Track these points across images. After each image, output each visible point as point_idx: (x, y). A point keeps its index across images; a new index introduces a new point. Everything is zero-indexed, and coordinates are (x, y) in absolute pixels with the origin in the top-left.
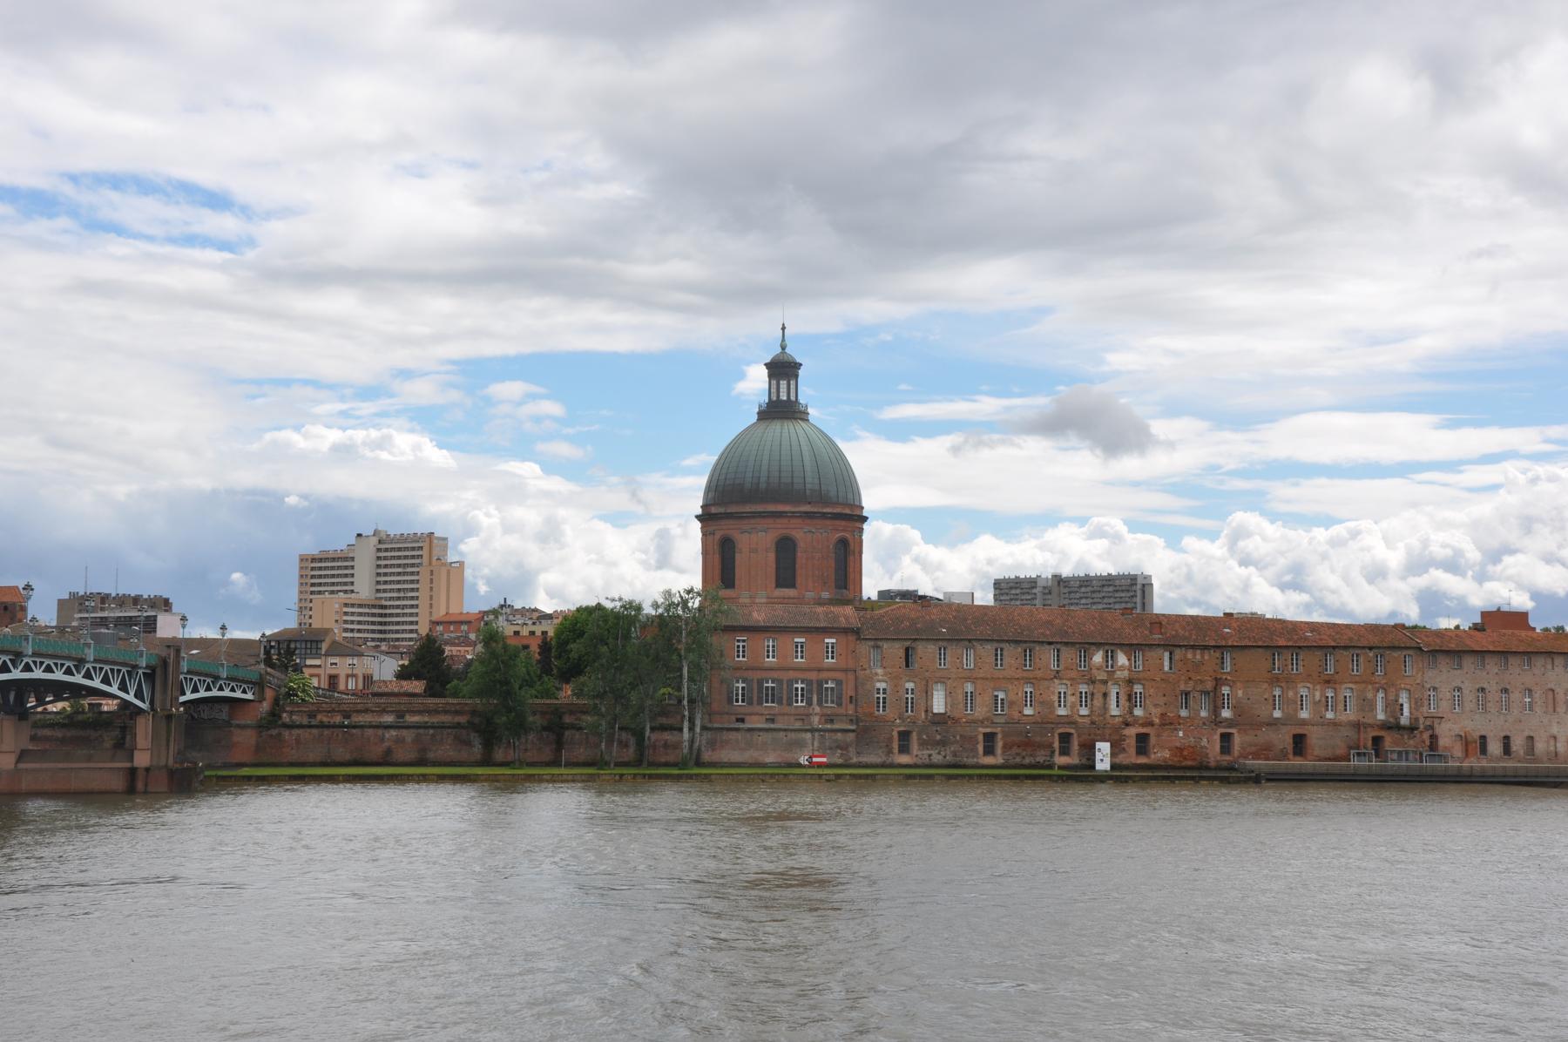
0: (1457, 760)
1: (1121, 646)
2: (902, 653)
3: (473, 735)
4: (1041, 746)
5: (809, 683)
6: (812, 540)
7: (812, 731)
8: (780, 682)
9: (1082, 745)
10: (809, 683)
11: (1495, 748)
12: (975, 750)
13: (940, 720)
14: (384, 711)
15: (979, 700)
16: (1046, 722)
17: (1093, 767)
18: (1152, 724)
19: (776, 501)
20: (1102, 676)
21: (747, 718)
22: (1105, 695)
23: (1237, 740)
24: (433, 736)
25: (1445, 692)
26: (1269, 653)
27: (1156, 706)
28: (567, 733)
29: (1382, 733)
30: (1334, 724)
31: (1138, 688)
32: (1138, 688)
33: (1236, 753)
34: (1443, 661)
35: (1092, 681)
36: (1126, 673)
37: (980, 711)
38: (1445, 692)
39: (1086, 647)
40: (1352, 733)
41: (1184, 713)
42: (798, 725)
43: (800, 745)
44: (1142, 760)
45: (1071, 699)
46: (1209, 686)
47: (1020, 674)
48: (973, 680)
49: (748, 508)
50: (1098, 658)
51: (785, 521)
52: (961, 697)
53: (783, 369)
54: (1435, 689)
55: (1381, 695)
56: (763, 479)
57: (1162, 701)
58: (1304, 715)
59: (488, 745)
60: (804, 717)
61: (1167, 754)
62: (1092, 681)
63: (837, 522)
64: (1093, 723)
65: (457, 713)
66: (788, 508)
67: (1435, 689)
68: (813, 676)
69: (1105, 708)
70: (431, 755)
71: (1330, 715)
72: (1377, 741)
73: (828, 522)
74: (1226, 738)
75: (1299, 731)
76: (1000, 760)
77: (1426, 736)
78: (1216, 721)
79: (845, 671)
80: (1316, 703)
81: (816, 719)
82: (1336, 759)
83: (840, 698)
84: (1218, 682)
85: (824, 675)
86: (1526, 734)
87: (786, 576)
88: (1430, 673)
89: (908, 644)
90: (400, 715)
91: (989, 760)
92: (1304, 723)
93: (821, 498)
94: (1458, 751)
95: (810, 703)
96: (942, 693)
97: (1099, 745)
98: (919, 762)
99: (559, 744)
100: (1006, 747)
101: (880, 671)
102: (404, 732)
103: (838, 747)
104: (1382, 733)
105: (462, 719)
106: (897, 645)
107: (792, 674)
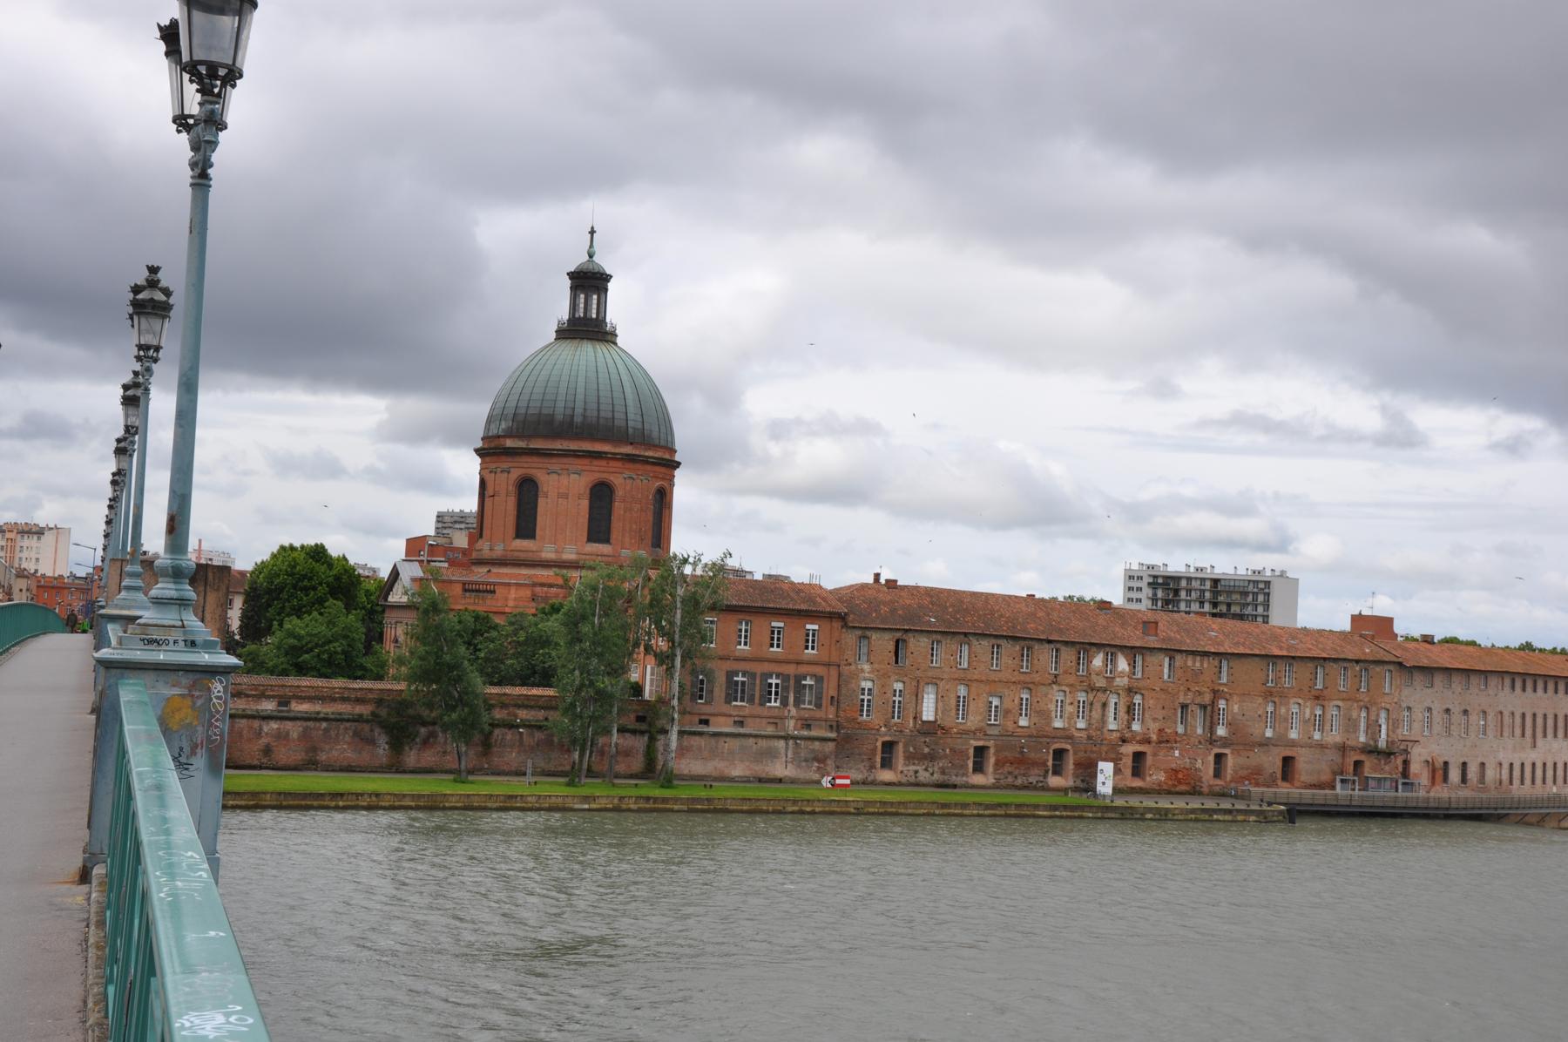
0: (1424, 791)
1: (1122, 648)
2: (892, 647)
3: (377, 731)
4: (1035, 764)
5: (785, 677)
6: (628, 485)
7: (786, 738)
8: (752, 676)
9: (1077, 765)
10: (785, 677)
11: (1454, 775)
12: (964, 766)
13: (930, 729)
14: (262, 696)
15: (972, 706)
16: (1040, 736)
17: (1094, 790)
18: (1149, 742)
19: (592, 438)
20: (1101, 683)
21: (712, 720)
22: (1104, 705)
23: (1230, 762)
24: (326, 730)
25: (1418, 714)
26: (1311, 665)
27: (1155, 719)
28: (497, 732)
29: (1362, 757)
30: (1321, 746)
31: (1137, 699)
32: (1137, 699)
33: (1229, 778)
34: (1418, 678)
35: (1092, 689)
36: (1126, 680)
37: (973, 721)
38: (1418, 714)
39: (1086, 648)
40: (1337, 757)
41: (1180, 729)
42: (770, 730)
43: (771, 754)
44: (1137, 783)
45: (1069, 709)
46: (1207, 699)
47: (1017, 677)
48: (968, 683)
49: (558, 445)
50: (1098, 661)
51: (603, 463)
52: (953, 702)
54: (1409, 708)
55: (1363, 714)
56: (579, 411)
57: (1160, 714)
58: (1293, 735)
59: (397, 745)
60: (777, 720)
61: (1162, 777)
62: (1092, 689)
63: (657, 469)
64: (1089, 738)
65: (359, 701)
66: (606, 448)
67: (1409, 708)
68: (790, 670)
69: (1103, 721)
70: (323, 757)
71: (1317, 736)
72: (1358, 764)
73: (649, 467)
75: (1288, 753)
76: (991, 780)
77: (1399, 761)
78: (1212, 740)
79: (828, 665)
80: (1306, 722)
81: (791, 726)
82: (1320, 786)
83: (819, 698)
84: (1216, 694)
85: (803, 669)
86: (1480, 760)
87: (599, 530)
88: (1406, 692)
89: (898, 635)
90: (284, 702)
91: (978, 779)
92: (1293, 744)
93: (643, 439)
94: (1424, 779)
95: (785, 703)
96: (932, 696)
97: (1101, 765)
98: (904, 780)
99: (487, 745)
100: (999, 764)
101: (867, 667)
102: (289, 725)
103: (816, 759)
104: (1362, 757)
105: (364, 710)
106: (887, 636)
107: (766, 667)
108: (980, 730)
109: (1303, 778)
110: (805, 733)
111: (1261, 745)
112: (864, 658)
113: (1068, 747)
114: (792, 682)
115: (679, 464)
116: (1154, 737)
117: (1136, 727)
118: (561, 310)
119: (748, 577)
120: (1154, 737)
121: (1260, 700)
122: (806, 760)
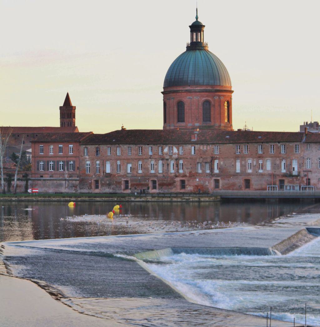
2: (95, 150)
7: (65, 180)
13: (109, 175)
16: (146, 176)
20: (167, 157)
21: (44, 176)
23: (221, 182)
27: (187, 169)
29: (284, 178)
42: (61, 178)
43: (61, 185)
44: (182, 191)
53: (196, 28)
64: (164, 176)
68: (65, 159)
71: (261, 171)
72: (282, 182)
73: (198, 94)
74: (217, 181)
75: (247, 178)
77: (305, 179)
81: (66, 176)
85: (69, 159)
92: (249, 174)
96: (109, 165)
101: (87, 157)
103: (74, 186)
108: (125, 175)
109: (254, 187)
110: (71, 179)
111: (234, 175)
112: (86, 154)
113: (156, 179)
114: (66, 163)
115: (233, 91)
116: (188, 175)
117: (181, 171)
118: (188, 40)
119: (125, 129)
120: (188, 175)
121: (233, 159)
122: (71, 187)
